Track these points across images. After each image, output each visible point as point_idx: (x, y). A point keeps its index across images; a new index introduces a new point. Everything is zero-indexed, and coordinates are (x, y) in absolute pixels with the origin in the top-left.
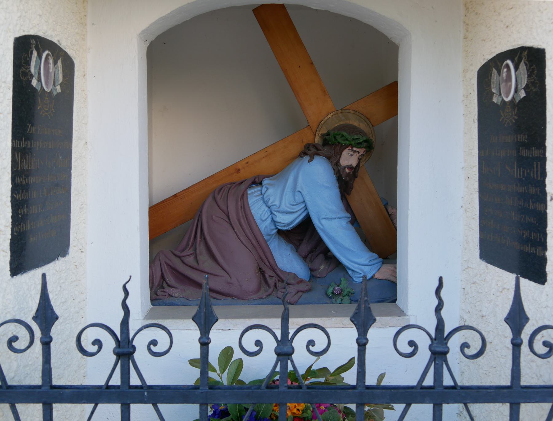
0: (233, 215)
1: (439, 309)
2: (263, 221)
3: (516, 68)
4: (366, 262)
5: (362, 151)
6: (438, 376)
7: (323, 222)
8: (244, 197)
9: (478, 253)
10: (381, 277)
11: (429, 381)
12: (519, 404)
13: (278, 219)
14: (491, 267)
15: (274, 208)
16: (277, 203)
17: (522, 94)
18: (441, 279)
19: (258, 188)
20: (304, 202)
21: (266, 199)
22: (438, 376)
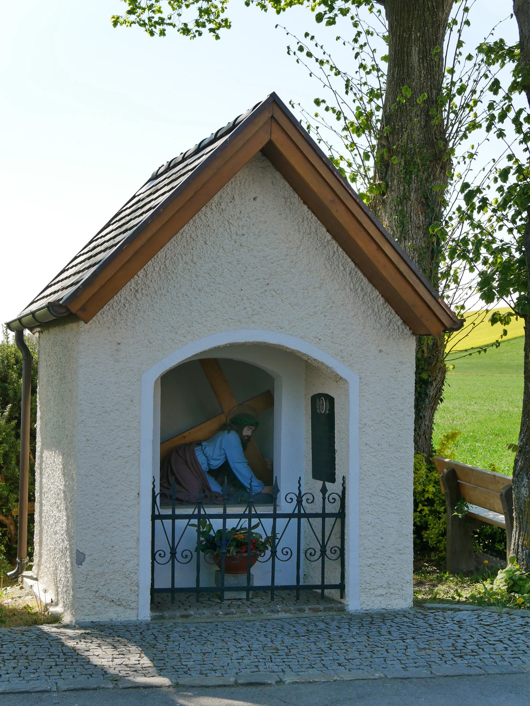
0: (189, 463)
1: (299, 488)
2: (203, 464)
3: (325, 402)
4: (257, 485)
5: (254, 428)
6: (299, 510)
7: (236, 464)
8: (193, 453)
9: (311, 477)
10: (265, 492)
11: (296, 512)
12: (325, 518)
13: (211, 463)
14: (317, 481)
15: (209, 457)
16: (211, 455)
17: (328, 412)
18: (300, 478)
19: (200, 447)
20: (225, 454)
21: (205, 453)
22: (299, 510)
